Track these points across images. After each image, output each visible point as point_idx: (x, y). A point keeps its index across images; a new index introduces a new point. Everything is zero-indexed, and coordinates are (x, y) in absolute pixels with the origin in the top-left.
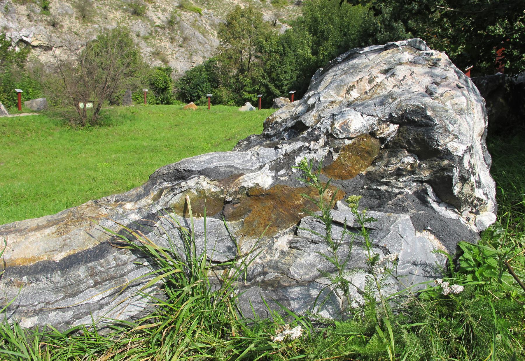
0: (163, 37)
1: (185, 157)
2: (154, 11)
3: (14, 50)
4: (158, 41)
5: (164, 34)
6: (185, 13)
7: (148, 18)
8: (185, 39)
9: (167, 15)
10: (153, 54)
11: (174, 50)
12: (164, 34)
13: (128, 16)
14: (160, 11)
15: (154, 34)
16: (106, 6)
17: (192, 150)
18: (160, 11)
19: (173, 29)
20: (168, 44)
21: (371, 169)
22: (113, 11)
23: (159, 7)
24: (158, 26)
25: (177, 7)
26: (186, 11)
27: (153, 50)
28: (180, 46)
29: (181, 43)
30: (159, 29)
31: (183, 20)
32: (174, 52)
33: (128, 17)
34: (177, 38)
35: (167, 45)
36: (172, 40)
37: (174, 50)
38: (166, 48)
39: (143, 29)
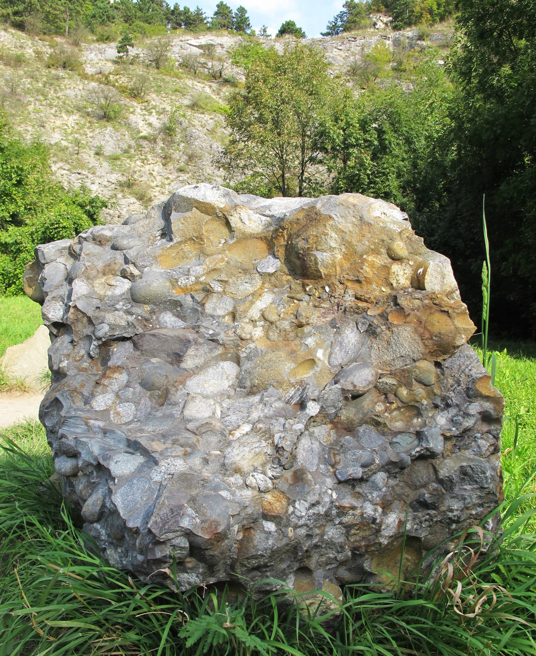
0: (149, 156)
1: (28, 597)
2: (144, 115)
3: (143, 50)
4: (139, 163)
5: (153, 150)
6: (202, 116)
7: (128, 125)
8: (191, 158)
9: (165, 119)
10: (121, 185)
11: (168, 178)
12: (153, 150)
13: (90, 122)
14: (154, 114)
15: (132, 151)
16: (51, 108)
17: (81, 537)
18: (154, 114)
19: (172, 142)
20: (158, 168)
21: (38, 525)
22: (63, 115)
23: (154, 108)
24: (145, 138)
25: (188, 106)
26: (203, 113)
27: (123, 179)
28: (181, 170)
29: (182, 164)
30: (144, 143)
31: (194, 126)
32: (167, 182)
33: (88, 124)
34: (176, 155)
35: (156, 169)
36: (166, 159)
37: (168, 178)
38: (151, 174)
39: (112, 143)
